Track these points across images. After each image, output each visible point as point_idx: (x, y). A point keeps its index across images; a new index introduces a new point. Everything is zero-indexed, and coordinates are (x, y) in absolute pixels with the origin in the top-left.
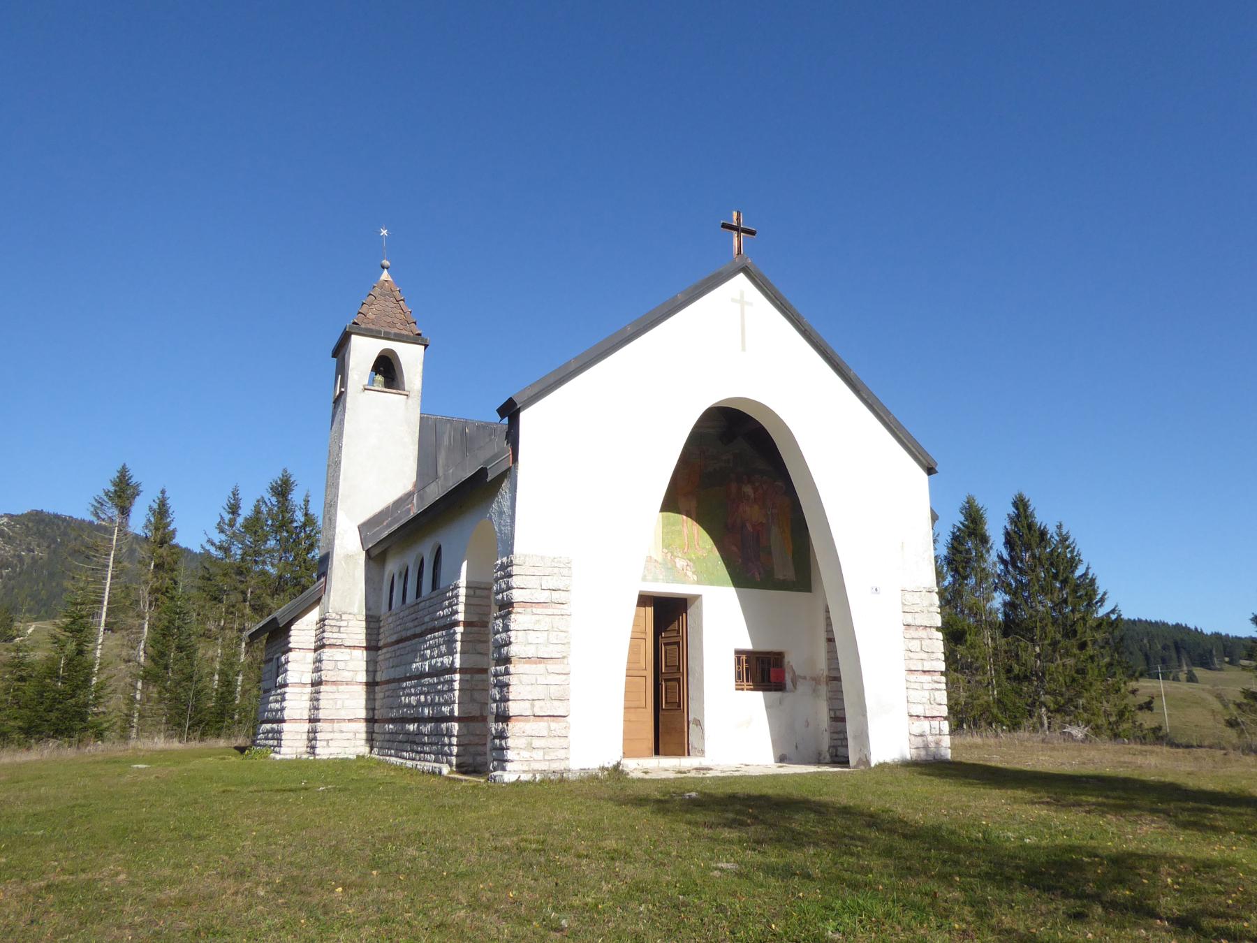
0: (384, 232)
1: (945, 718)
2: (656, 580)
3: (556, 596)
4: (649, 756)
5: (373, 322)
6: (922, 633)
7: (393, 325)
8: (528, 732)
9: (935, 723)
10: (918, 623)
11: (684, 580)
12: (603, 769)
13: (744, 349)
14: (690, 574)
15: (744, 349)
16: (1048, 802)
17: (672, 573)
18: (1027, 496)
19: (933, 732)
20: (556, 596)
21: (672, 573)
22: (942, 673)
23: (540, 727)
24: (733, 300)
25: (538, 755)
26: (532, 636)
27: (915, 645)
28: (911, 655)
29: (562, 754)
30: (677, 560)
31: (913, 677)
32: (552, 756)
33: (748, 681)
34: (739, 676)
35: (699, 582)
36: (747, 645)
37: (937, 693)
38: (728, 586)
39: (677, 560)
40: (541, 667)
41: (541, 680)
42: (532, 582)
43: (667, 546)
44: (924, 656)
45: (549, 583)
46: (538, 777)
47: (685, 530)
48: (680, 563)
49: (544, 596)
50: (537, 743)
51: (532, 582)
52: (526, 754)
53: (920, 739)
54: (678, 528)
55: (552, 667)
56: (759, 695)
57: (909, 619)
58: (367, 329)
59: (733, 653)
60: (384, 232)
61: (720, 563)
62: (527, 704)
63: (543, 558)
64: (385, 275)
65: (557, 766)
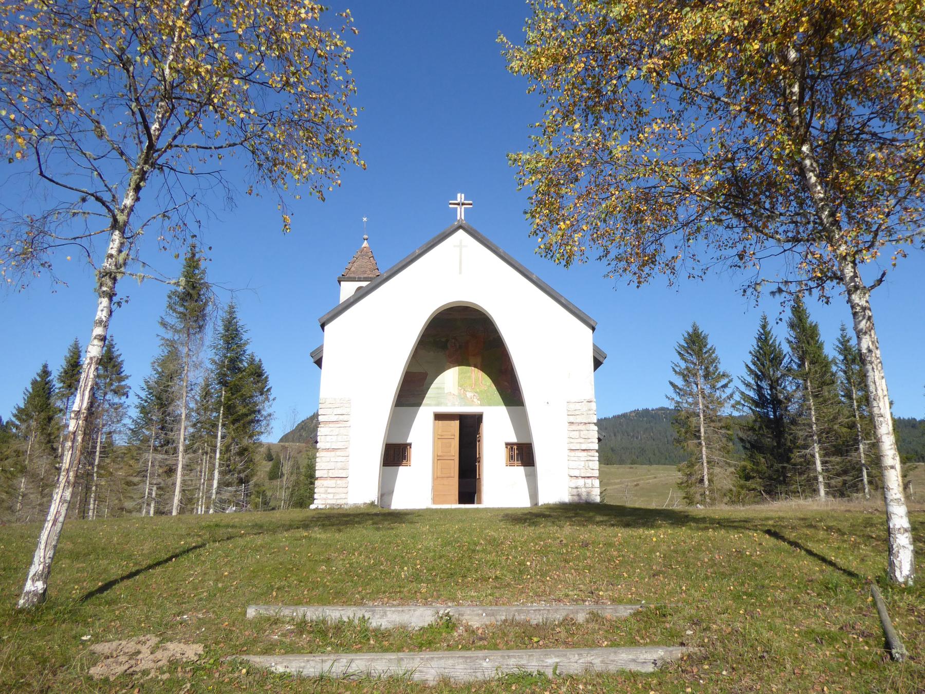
0: (365, 219)
1: (597, 478)
2: (454, 405)
3: (341, 418)
4: (456, 503)
5: (354, 272)
6: (582, 427)
7: (365, 272)
8: (325, 485)
9: (589, 481)
10: (579, 421)
11: (472, 404)
12: (365, 504)
13: (460, 273)
14: (475, 400)
15: (460, 273)
16: (602, 521)
17: (464, 400)
18: (703, 329)
19: (587, 486)
20: (341, 418)
21: (464, 400)
22: (597, 451)
23: (332, 483)
24: (455, 246)
25: (330, 496)
26: (328, 438)
27: (576, 434)
28: (572, 440)
29: (343, 496)
30: (467, 393)
31: (573, 454)
32: (338, 497)
33: (517, 461)
34: (511, 458)
35: (481, 405)
36: (513, 439)
37: (591, 463)
38: (498, 405)
39: (467, 393)
40: (333, 453)
41: (333, 459)
42: (329, 411)
43: (461, 385)
44: (582, 441)
45: (339, 411)
46: (328, 507)
47: (473, 375)
48: (469, 395)
49: (334, 418)
50: (330, 490)
51: (329, 411)
52: (324, 496)
53: (575, 490)
54: (469, 375)
55: (338, 453)
56: (522, 468)
57: (572, 419)
58: (348, 278)
59: (504, 446)
60: (365, 219)
61: (496, 392)
62: (325, 472)
63: (335, 399)
64: (365, 244)
65: (339, 502)
